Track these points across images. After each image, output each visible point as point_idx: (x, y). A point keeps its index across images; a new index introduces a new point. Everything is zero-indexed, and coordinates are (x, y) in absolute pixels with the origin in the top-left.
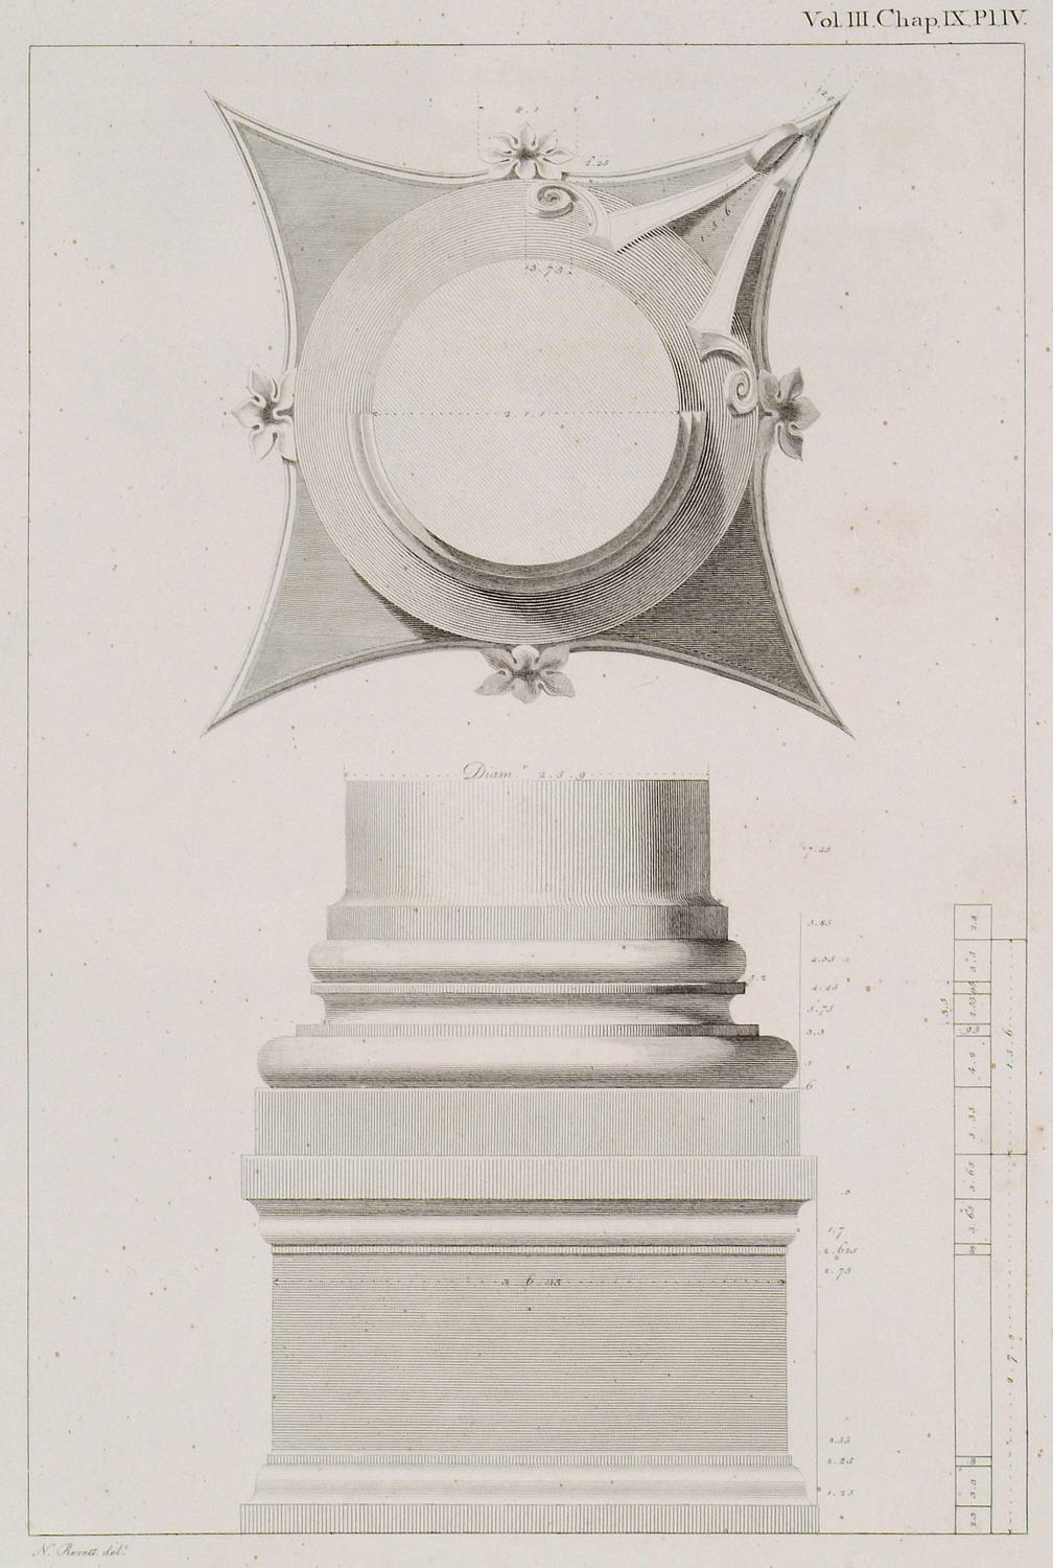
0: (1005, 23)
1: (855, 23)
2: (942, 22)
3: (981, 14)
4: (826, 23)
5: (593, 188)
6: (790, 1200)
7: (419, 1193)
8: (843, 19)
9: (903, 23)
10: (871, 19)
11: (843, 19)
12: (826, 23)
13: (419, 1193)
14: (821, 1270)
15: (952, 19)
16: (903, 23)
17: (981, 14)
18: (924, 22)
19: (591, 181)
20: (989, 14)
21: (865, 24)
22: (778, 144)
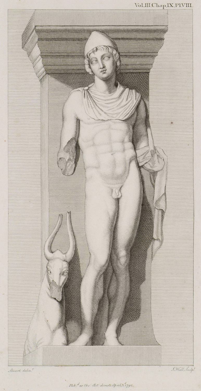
0: (180, 7)
2: (141, 6)
4: (140, 6)
8: (144, 5)
10: (151, 5)
12: (140, 6)
15: (169, 5)
17: (177, 4)
18: (163, 6)
21: (191, 6)
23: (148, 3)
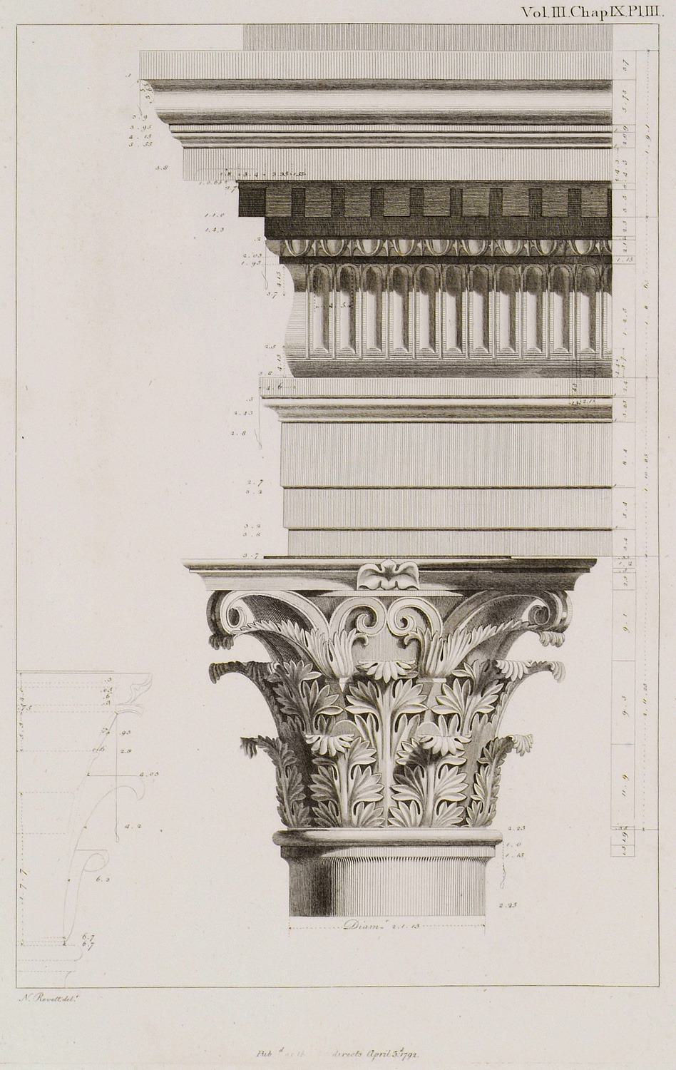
1: (654, 9)
2: (609, 14)
3: (633, 8)
4: (537, 14)
5: (414, 578)
6: (256, 79)
7: (229, 75)
8: (549, 12)
9: (585, 14)
10: (568, 13)
11: (549, 12)
12: (537, 14)
13: (229, 75)
14: (625, 400)
16: (585, 14)
17: (633, 8)
18: (599, 14)
19: (379, 566)
20: (638, 8)
21: (647, 7)
22: (318, 182)
23: (654, 4)
